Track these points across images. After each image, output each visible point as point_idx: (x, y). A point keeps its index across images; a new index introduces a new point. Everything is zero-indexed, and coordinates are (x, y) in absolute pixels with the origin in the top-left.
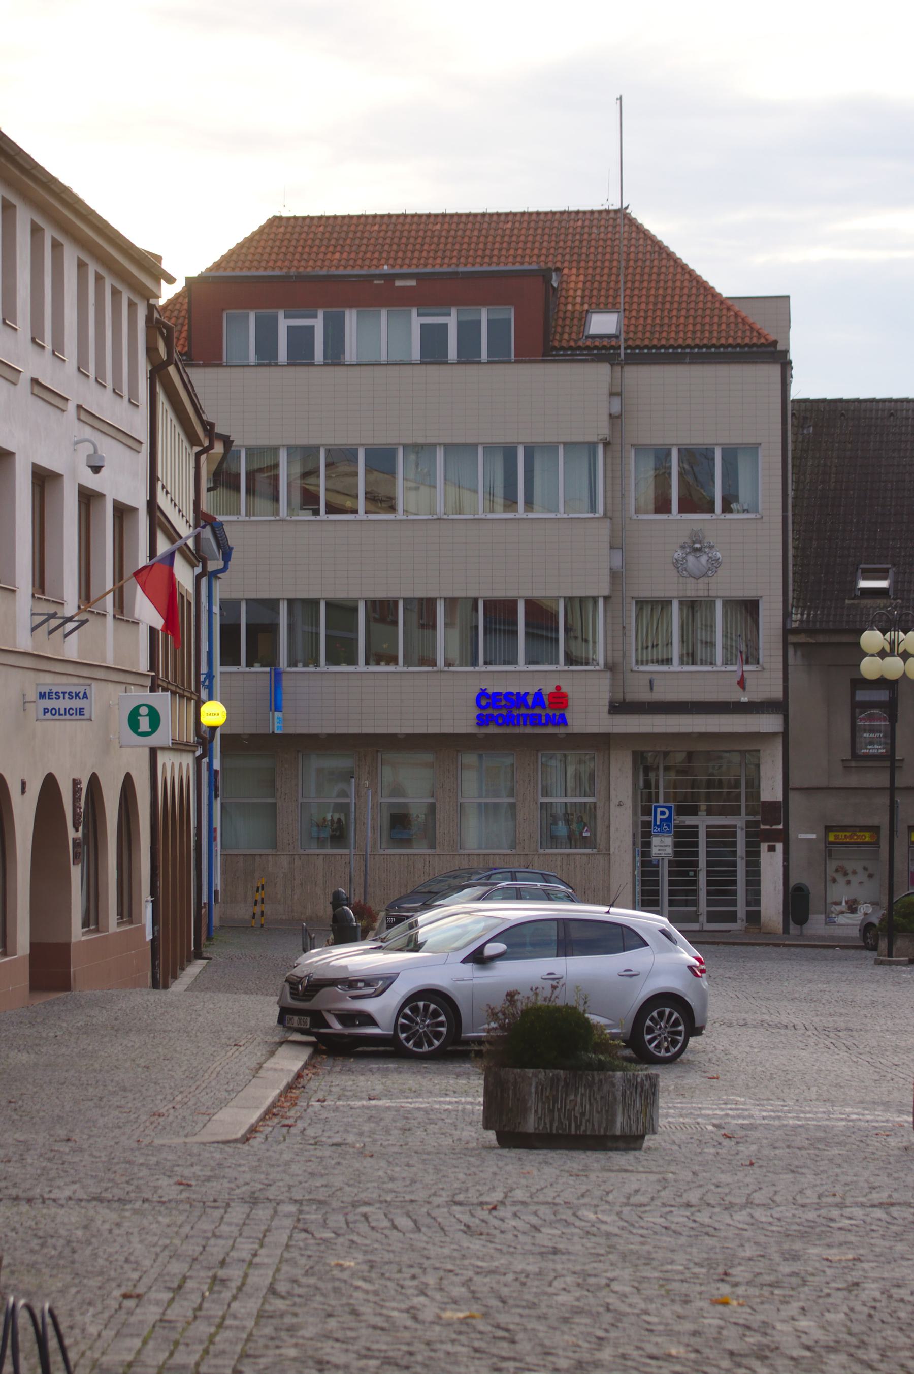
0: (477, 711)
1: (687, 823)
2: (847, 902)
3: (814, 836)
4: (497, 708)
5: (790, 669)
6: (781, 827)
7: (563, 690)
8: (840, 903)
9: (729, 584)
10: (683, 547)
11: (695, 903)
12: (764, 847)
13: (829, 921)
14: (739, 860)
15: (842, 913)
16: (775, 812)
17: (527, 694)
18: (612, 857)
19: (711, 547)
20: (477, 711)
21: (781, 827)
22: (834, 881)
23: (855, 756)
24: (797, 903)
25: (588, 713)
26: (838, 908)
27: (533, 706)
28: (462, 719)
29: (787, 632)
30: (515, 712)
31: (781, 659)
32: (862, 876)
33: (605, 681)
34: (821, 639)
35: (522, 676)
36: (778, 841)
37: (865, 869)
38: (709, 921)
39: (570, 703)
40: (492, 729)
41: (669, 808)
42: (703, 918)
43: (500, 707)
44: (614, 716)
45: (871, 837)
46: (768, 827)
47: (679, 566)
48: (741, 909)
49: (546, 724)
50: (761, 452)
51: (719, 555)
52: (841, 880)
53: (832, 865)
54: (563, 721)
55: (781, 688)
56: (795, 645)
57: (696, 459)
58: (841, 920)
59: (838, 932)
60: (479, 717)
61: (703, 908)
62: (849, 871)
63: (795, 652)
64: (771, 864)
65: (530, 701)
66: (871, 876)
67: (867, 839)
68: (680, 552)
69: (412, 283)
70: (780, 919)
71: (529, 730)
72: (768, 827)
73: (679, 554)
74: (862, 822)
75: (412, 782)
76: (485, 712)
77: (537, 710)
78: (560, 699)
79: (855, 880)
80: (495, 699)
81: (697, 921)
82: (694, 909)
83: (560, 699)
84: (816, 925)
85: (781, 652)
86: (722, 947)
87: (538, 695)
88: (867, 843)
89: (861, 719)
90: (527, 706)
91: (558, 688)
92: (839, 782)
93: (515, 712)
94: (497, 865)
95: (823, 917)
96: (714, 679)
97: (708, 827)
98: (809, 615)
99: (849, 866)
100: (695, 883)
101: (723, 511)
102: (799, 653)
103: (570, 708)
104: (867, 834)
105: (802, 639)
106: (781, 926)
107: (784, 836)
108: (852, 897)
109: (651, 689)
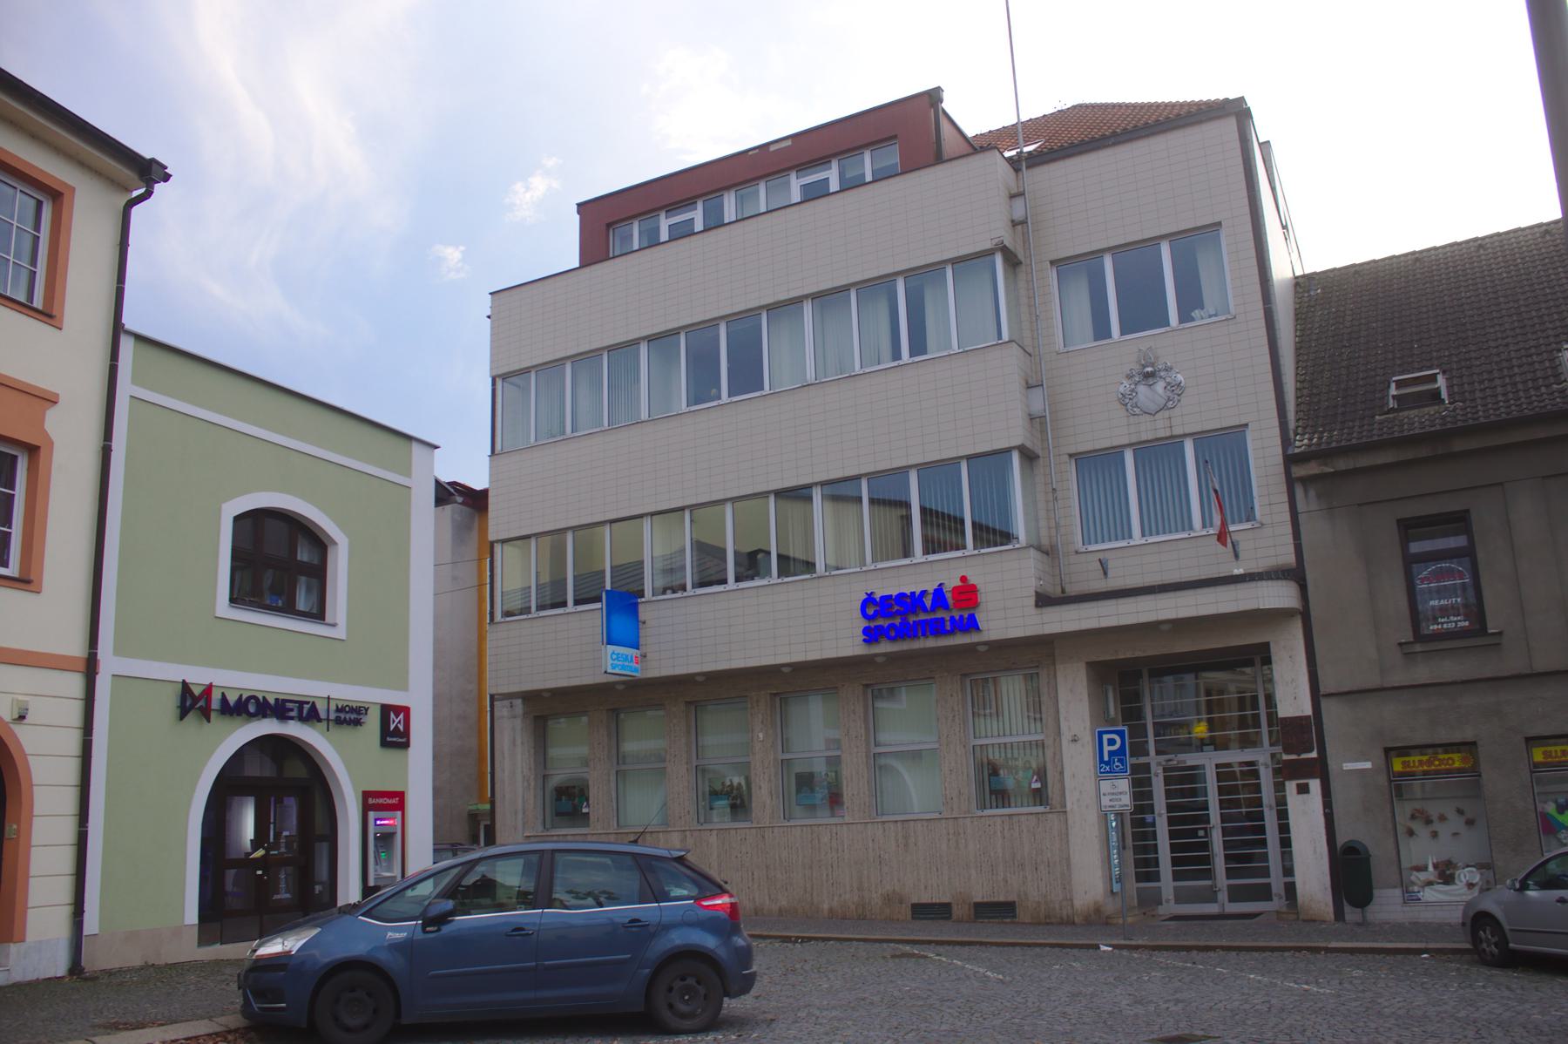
0: (864, 623)
1: (1189, 763)
2: (1435, 866)
3: (1368, 765)
4: (889, 616)
5: (1302, 518)
6: (1314, 755)
7: (972, 580)
8: (1424, 868)
9: (1193, 417)
10: (1129, 377)
11: (1208, 874)
12: (1291, 786)
13: (1410, 898)
14: (1164, 811)
15: (1430, 883)
16: (1297, 733)
17: (923, 593)
18: (1070, 816)
19: (1168, 369)
20: (864, 623)
21: (1314, 755)
22: (1411, 833)
23: (1419, 637)
24: (1352, 872)
25: (1008, 611)
26: (1422, 876)
27: (933, 609)
28: (842, 637)
29: (1290, 460)
30: (912, 619)
31: (1286, 507)
32: (1455, 823)
33: (1032, 561)
34: (1342, 464)
35: (921, 573)
36: (1312, 776)
37: (1460, 812)
38: (1178, 900)
39: (982, 598)
40: (885, 647)
41: (1121, 734)
42: (1223, 896)
43: (890, 615)
44: (1045, 610)
45: (1464, 760)
46: (1294, 757)
47: (1126, 401)
48: (1276, 881)
49: (951, 632)
50: (1223, 233)
51: (1180, 377)
52: (1422, 831)
53: (1403, 811)
54: (971, 625)
55: (1291, 549)
56: (1306, 481)
57: (1136, 258)
58: (1429, 894)
59: (1426, 916)
60: (866, 631)
61: (1222, 880)
62: (1435, 818)
63: (1306, 492)
64: (1306, 812)
65: (928, 601)
66: (1470, 823)
67: (1457, 765)
68: (1126, 383)
69: (789, 143)
70: (1328, 898)
71: (931, 642)
72: (1294, 757)
73: (1125, 387)
74: (1443, 736)
75: (817, 729)
76: (872, 624)
77: (940, 614)
78: (967, 593)
79: (1444, 830)
80: (912, 602)
81: (1214, 900)
82: (1208, 883)
83: (967, 593)
84: (1387, 905)
85: (1285, 498)
86: (1244, 956)
87: (939, 592)
88: (1459, 770)
89: (1423, 580)
90: (925, 610)
91: (964, 579)
92: (1398, 678)
93: (912, 619)
94: (999, 820)
95: (1398, 892)
96: (1191, 550)
97: (1218, 766)
98: (1320, 438)
99: (1434, 810)
100: (1205, 846)
101: (1181, 322)
102: (1312, 493)
103: (982, 606)
104: (1456, 756)
105: (1312, 469)
106: (1331, 909)
107: (1319, 768)
108: (1444, 857)
109: (1105, 574)
